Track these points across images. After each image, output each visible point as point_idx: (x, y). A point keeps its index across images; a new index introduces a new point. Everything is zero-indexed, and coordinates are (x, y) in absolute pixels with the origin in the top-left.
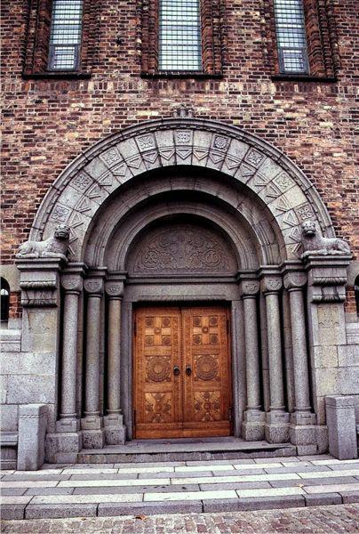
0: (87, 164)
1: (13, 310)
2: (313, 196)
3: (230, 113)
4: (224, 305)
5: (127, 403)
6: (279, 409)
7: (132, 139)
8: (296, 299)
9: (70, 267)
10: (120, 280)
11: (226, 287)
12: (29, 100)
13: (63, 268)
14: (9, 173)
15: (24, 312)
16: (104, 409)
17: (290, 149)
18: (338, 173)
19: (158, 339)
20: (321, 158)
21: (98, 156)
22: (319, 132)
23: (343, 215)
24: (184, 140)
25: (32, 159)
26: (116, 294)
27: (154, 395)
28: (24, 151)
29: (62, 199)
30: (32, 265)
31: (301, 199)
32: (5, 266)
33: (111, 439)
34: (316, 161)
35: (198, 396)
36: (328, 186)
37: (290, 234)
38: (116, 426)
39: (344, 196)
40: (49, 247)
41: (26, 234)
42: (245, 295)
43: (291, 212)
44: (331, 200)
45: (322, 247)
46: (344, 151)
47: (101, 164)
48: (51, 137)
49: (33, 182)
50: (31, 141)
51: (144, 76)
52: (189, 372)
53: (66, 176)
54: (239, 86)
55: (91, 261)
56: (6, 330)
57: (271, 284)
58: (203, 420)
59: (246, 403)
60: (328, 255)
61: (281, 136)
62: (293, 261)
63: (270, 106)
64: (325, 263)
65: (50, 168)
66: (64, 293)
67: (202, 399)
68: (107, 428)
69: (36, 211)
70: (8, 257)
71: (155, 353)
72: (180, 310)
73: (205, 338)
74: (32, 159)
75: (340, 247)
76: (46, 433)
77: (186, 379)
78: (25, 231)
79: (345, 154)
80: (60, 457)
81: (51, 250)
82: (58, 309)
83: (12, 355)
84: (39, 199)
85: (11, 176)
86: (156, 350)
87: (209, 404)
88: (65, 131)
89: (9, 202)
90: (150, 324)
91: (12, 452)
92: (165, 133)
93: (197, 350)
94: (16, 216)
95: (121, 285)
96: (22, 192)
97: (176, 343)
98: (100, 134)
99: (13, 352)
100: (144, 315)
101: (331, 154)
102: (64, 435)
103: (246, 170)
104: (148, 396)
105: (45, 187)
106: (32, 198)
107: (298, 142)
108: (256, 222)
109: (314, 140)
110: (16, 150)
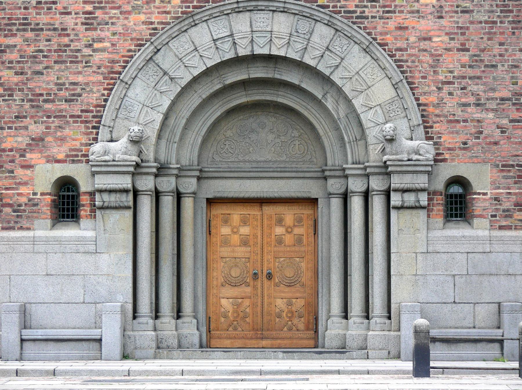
0: (156, 53)
1: (86, 211)
2: (404, 91)
4: (313, 202)
5: (201, 308)
6: (358, 316)
7: (204, 23)
8: (377, 204)
9: (143, 167)
10: (193, 176)
11: (311, 182)
13: (138, 169)
14: (71, 62)
15: (98, 212)
16: (178, 314)
17: (381, 34)
18: (437, 58)
19: (235, 239)
20: (417, 44)
21: (167, 43)
22: (418, 12)
23: (437, 112)
24: (262, 25)
25: (96, 45)
26: (189, 191)
27: (231, 300)
28: (86, 36)
29: (130, 93)
30: (109, 167)
32: (74, 165)
33: (184, 342)
34: (413, 48)
35: (280, 303)
36: (424, 77)
37: (373, 134)
38: (190, 329)
39: (439, 89)
40: (123, 150)
41: (94, 131)
42: (330, 194)
43: (378, 108)
44: (425, 93)
45: (402, 152)
46: (447, 34)
47: (171, 54)
48: (114, 20)
49: (98, 73)
50: (92, 24)
52: (270, 276)
53: (134, 68)
55: (162, 158)
56: (79, 231)
57: (356, 185)
58: (285, 329)
59: (329, 311)
60: (409, 160)
61: (373, 17)
62: (375, 164)
64: (404, 169)
65: (117, 58)
66: (136, 193)
67: (284, 307)
68: (180, 331)
69: (104, 106)
70: (77, 156)
71: (232, 255)
72: (261, 206)
73: (288, 239)
74: (96, 45)
75: (421, 152)
76: (124, 331)
77: (266, 283)
78: (94, 127)
79: (446, 38)
80: (138, 353)
81: (126, 153)
82: (132, 209)
83: (88, 256)
84: (106, 92)
85: (74, 66)
86: (233, 251)
87: (292, 312)
88: (129, 13)
89: (74, 95)
90: (226, 222)
91: (96, 345)
92: (241, 15)
93: (279, 252)
94: (82, 111)
95: (194, 181)
96: (87, 84)
97: (256, 244)
98: (169, 16)
99: (88, 253)
100: (219, 211)
101: (430, 39)
102: (141, 333)
103: (331, 60)
104: (224, 302)
105: (112, 78)
106: (98, 91)
107: (392, 24)
108: (342, 114)
109: (410, 21)
110: (76, 35)
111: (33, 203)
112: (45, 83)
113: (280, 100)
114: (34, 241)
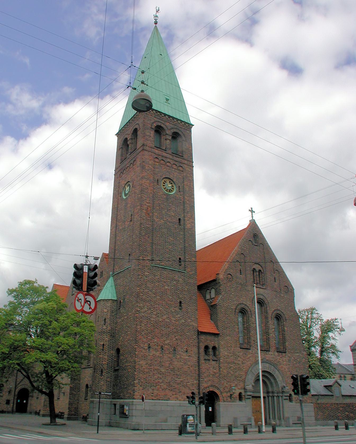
59: (270, 417)
112: (237, 374)
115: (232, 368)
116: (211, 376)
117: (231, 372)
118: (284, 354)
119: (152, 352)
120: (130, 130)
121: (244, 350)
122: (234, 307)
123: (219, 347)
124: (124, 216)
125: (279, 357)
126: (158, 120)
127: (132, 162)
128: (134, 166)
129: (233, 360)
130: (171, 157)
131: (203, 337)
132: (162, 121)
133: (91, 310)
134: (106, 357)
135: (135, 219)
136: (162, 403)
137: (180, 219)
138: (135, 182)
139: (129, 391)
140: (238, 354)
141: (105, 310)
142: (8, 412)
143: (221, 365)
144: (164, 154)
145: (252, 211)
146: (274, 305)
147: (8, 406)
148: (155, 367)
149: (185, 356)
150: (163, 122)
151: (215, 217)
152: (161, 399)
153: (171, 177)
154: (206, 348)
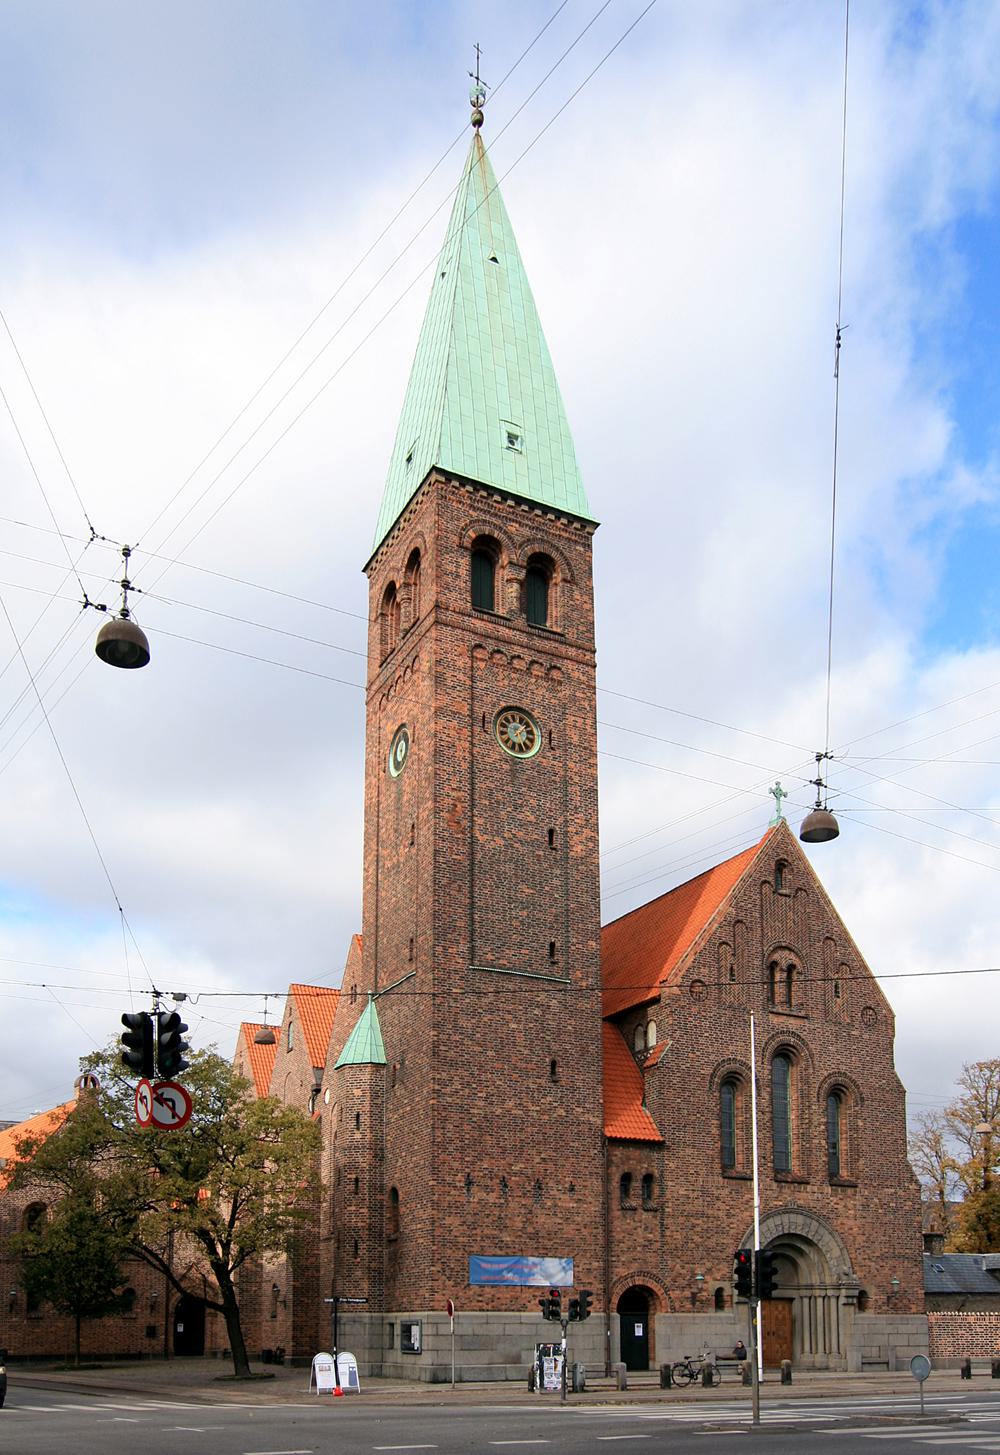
3: (812, 1205)
12: (727, 1191)
31: (839, 1253)
51: (776, 1181)
54: (815, 1189)
59: (803, 1348)
63: (828, 1201)
103: (818, 1237)
107: (839, 1222)
111: (708, 1300)
112: (711, 1243)
113: (787, 1253)
114: (710, 1318)
115: (698, 1229)
116: (639, 1249)
117: (696, 1238)
118: (850, 1191)
119: (478, 1194)
120: (400, 558)
121: (734, 1182)
122: (708, 1071)
123: (662, 1176)
124: (396, 831)
125: (835, 1200)
126: (483, 517)
127: (408, 662)
128: (415, 677)
129: (700, 1209)
130: (524, 639)
131: (619, 1153)
132: (494, 520)
133: (177, 1120)
134: (365, 1210)
135: (422, 840)
136: (506, 1317)
137: (551, 832)
138: (418, 726)
139: (421, 1292)
140: (716, 1193)
141: (357, 1092)
142: (156, 1356)
143: (668, 1221)
144: (504, 632)
145: (778, 793)
146: (828, 1057)
147: (154, 1342)
148: (486, 1231)
149: (567, 1202)
150: (498, 522)
151: (661, 815)
152: (504, 1307)
153: (525, 704)
154: (626, 1178)
